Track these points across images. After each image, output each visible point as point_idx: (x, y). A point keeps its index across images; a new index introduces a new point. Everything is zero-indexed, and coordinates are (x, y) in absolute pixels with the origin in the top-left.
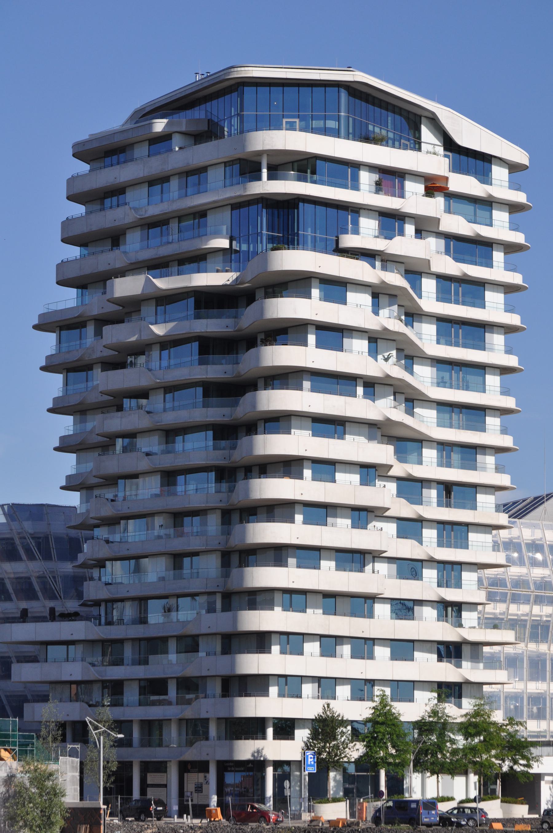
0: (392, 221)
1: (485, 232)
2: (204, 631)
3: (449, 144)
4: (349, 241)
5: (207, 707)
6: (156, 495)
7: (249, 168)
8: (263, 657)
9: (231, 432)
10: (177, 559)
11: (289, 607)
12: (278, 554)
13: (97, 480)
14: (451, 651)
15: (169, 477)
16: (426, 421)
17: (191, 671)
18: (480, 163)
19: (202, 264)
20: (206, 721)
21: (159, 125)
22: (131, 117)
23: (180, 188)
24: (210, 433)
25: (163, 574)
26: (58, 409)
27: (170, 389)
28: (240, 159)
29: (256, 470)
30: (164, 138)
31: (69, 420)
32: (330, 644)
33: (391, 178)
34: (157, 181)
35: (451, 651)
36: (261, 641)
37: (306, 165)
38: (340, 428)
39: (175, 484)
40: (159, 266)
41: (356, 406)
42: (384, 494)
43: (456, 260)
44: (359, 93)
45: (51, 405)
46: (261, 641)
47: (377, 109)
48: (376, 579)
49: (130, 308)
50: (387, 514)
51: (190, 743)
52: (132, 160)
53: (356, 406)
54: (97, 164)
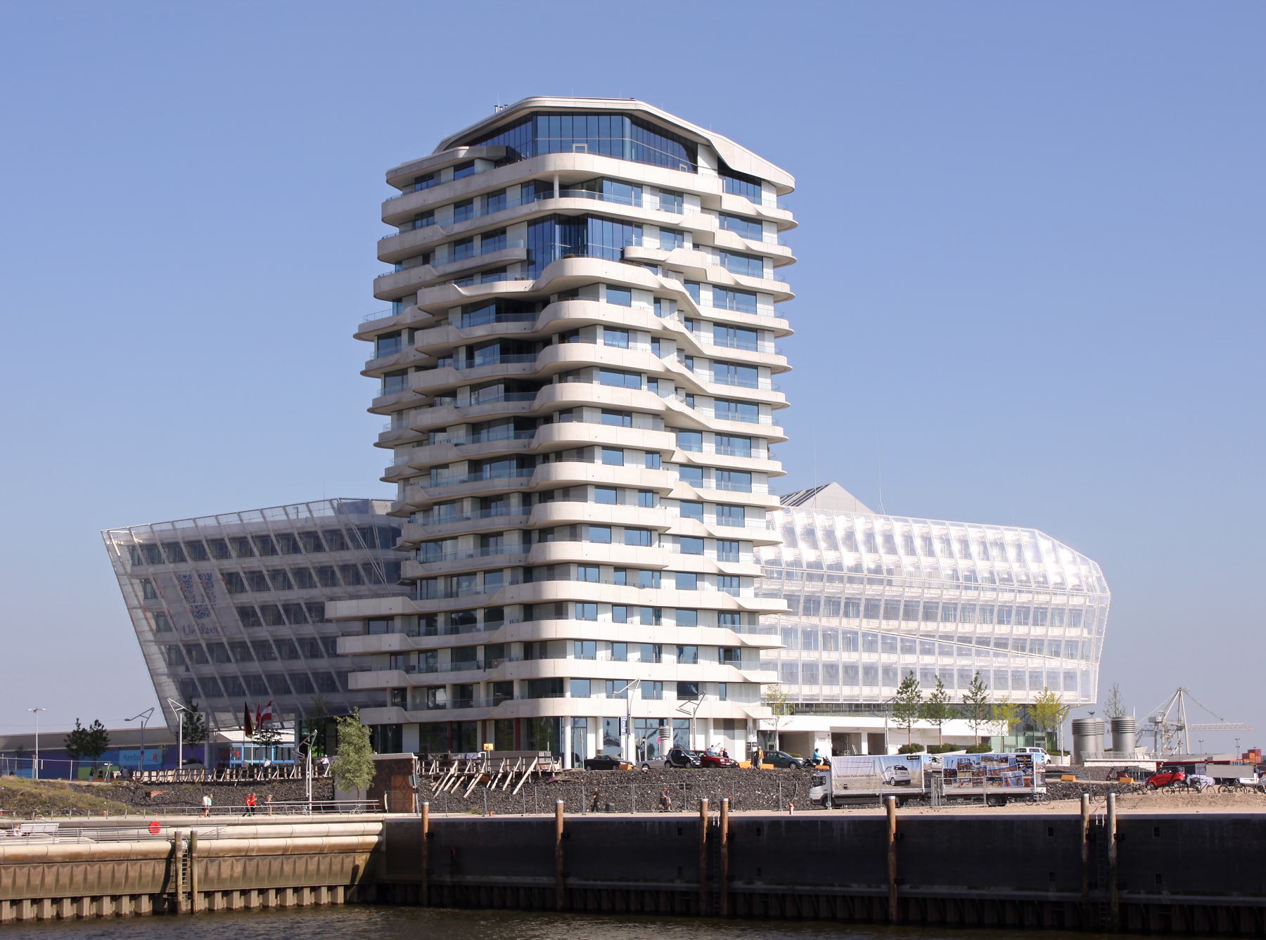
0: (674, 233)
1: (756, 246)
2: (507, 601)
3: (723, 169)
4: (634, 252)
5: (513, 670)
6: (464, 482)
7: (542, 188)
8: (559, 661)
9: (528, 387)
10: (484, 539)
11: (582, 616)
12: (573, 530)
13: (412, 471)
14: (726, 616)
15: (476, 466)
16: (705, 415)
17: (496, 601)
18: (751, 186)
19: (503, 275)
20: (511, 683)
21: (463, 152)
22: (439, 148)
23: (482, 207)
24: (512, 426)
25: (471, 552)
26: (382, 443)
27: (475, 387)
28: (535, 180)
29: (552, 456)
30: (466, 165)
31: (387, 420)
32: (623, 611)
33: (672, 195)
34: (462, 205)
35: (726, 616)
36: (559, 609)
37: (594, 184)
38: (627, 419)
39: (481, 470)
40: (464, 277)
41: (643, 398)
42: (666, 478)
43: (731, 271)
44: (642, 122)
45: (383, 475)
46: (559, 609)
47: (658, 137)
48: (664, 554)
49: (439, 316)
50: (671, 495)
51: (497, 703)
52: (439, 184)
53: (643, 398)
54: (407, 190)
